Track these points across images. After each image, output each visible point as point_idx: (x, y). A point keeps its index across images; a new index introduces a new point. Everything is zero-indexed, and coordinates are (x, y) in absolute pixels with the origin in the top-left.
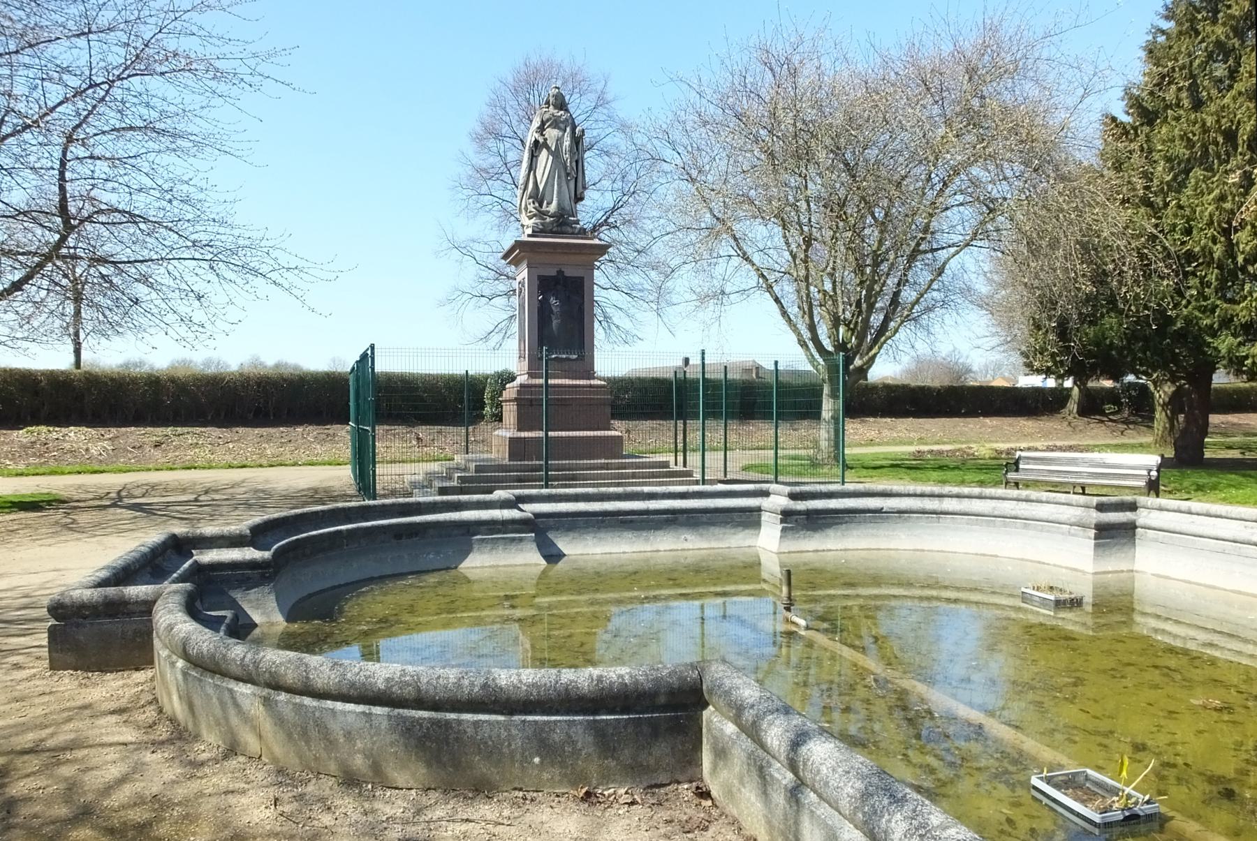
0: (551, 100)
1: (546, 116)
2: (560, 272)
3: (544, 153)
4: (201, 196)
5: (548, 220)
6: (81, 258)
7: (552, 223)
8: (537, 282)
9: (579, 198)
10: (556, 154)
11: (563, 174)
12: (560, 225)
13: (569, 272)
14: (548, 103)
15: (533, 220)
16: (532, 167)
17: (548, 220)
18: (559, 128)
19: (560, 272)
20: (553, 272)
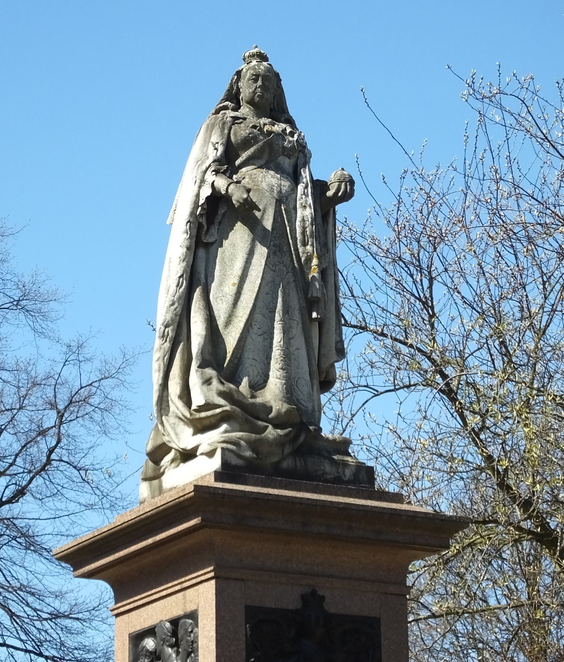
0: (246, 90)
1: (241, 132)
2: (312, 599)
3: (239, 237)
4: (83, 597)
5: (271, 433)
6: (479, 405)
7: (280, 442)
8: (242, 631)
9: (326, 383)
10: (277, 241)
11: (295, 303)
12: (298, 452)
13: (341, 601)
14: (233, 96)
15: (215, 436)
16: (197, 276)
17: (271, 433)
18: (279, 169)
19: (312, 599)
20: (287, 598)
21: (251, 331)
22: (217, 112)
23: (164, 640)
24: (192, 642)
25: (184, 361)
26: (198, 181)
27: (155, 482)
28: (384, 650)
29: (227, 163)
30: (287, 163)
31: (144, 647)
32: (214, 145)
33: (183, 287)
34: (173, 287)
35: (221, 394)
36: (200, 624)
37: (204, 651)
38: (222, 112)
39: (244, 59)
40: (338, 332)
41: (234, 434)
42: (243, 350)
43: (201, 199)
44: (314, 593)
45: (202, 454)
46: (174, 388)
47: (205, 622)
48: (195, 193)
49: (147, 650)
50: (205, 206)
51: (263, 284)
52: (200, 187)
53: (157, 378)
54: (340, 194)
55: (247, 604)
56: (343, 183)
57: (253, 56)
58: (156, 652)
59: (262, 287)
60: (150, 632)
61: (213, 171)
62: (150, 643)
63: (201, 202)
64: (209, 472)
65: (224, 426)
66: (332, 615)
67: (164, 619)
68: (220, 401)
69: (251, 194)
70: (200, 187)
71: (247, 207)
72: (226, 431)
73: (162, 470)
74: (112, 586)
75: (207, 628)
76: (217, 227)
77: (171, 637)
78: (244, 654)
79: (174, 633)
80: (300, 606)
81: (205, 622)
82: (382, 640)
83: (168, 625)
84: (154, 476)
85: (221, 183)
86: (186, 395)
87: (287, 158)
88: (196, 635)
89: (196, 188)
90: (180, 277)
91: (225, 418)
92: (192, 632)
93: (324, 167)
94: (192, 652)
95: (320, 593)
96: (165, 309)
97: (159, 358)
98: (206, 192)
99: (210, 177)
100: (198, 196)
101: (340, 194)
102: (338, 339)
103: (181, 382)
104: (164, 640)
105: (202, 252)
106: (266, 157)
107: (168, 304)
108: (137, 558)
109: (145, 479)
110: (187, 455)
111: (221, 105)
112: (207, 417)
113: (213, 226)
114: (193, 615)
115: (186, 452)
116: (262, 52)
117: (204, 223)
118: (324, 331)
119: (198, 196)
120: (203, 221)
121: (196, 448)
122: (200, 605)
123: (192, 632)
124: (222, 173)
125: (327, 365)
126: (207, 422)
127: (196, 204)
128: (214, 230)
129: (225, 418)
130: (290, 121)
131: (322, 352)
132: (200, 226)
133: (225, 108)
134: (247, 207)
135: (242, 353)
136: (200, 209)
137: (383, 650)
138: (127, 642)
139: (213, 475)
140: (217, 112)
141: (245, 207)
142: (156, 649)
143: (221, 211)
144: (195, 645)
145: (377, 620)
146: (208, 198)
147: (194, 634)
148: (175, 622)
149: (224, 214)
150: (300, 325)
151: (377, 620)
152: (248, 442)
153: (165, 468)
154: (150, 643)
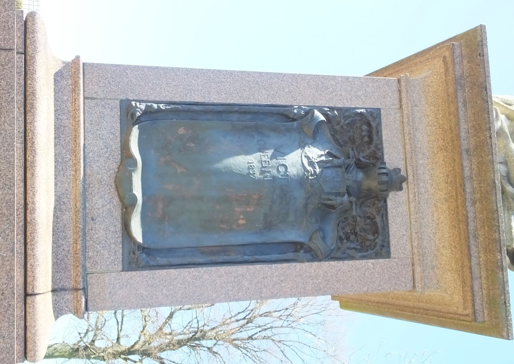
78: (340, 106)
95: (404, 185)
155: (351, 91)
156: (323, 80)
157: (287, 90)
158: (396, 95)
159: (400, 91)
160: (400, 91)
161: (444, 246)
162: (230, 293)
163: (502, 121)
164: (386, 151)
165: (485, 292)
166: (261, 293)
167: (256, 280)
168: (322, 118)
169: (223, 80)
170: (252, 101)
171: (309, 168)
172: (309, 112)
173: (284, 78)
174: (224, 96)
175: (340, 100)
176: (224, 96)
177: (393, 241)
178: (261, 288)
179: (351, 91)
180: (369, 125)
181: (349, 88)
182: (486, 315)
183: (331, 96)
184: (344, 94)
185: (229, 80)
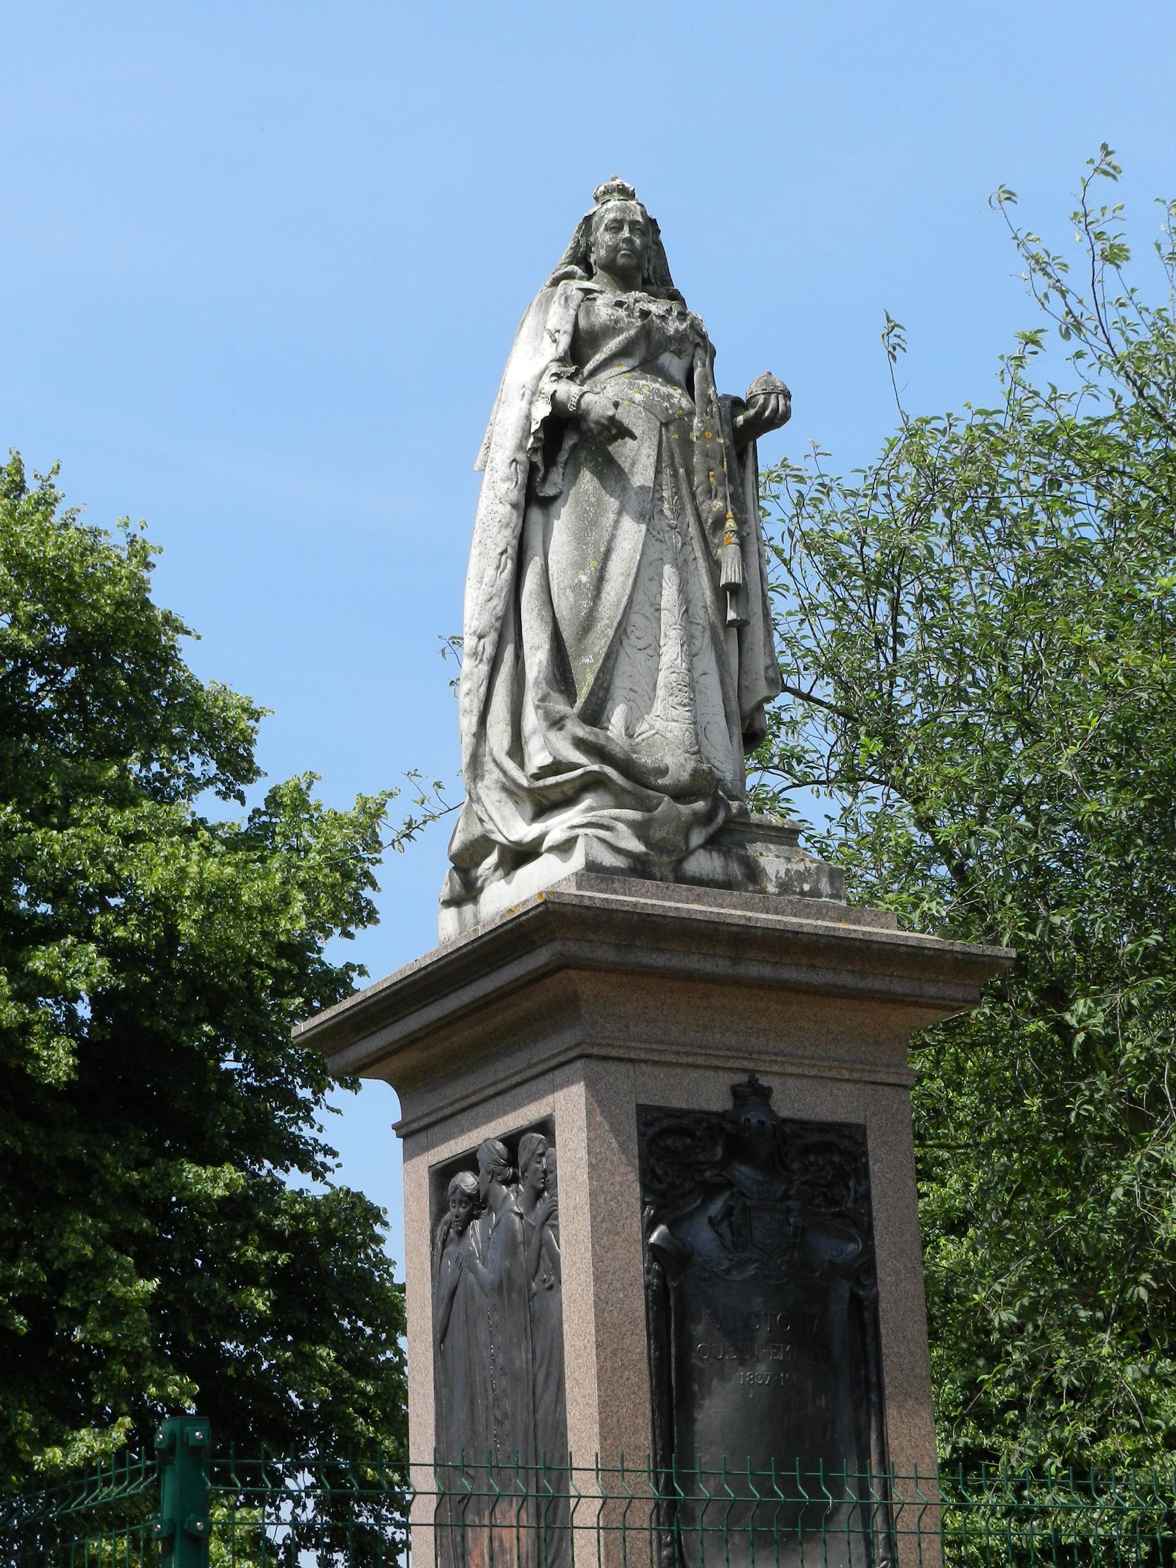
20: (710, 1094)
21: (625, 642)
22: (556, 282)
23: (493, 1174)
24: (545, 1172)
25: (546, 623)
26: (528, 393)
27: (468, 909)
28: (874, 1180)
29: (578, 351)
30: (672, 363)
31: (457, 1187)
32: (552, 335)
33: (506, 571)
34: (490, 572)
35: (580, 744)
36: (558, 1139)
37: (568, 1186)
38: (563, 283)
39: (597, 199)
40: (767, 650)
41: (606, 812)
42: (612, 674)
43: (533, 423)
44: (753, 1083)
45: (551, 849)
46: (499, 737)
47: (566, 1135)
48: (523, 413)
49: (463, 1193)
50: (541, 435)
51: (644, 563)
52: (531, 403)
53: (469, 724)
54: (767, 413)
55: (640, 1102)
56: (773, 396)
57: (608, 191)
58: (478, 1191)
59: (642, 569)
60: (468, 1161)
61: (553, 375)
62: (467, 1181)
63: (535, 427)
64: (565, 875)
65: (588, 801)
66: (785, 1121)
67: (492, 1136)
68: (577, 757)
69: (620, 410)
70: (531, 403)
71: (614, 431)
72: (591, 809)
73: (479, 883)
74: (397, 1088)
75: (572, 1146)
76: (561, 470)
77: (505, 1166)
78: (638, 1189)
79: (512, 1160)
80: (729, 1105)
81: (566, 1135)
82: (871, 1163)
83: (500, 1146)
84: (466, 892)
85: (568, 391)
86: (517, 750)
87: (676, 358)
88: (551, 1160)
89: (524, 404)
90: (502, 554)
91: (592, 783)
92: (542, 1155)
93: (734, 377)
94: (543, 1190)
95: (764, 1081)
96: (478, 609)
97: (470, 690)
98: (543, 410)
99: (548, 386)
100: (528, 417)
101: (767, 413)
102: (769, 662)
103: (509, 728)
104: (493, 1174)
105: (536, 515)
106: (641, 352)
107: (481, 599)
108: (442, 1033)
109: (447, 903)
110: (519, 856)
111: (562, 271)
112: (558, 784)
113: (554, 469)
114: (545, 1127)
115: (518, 848)
116: (627, 185)
117: (540, 464)
118: (746, 646)
119: (528, 417)
120: (538, 459)
121: (541, 839)
122: (558, 1106)
123: (542, 1155)
124: (568, 378)
125: (753, 704)
126: (555, 796)
127: (527, 432)
128: (556, 475)
129: (592, 783)
130: (675, 296)
131: (743, 683)
132: (532, 469)
133: (569, 276)
134: (614, 431)
135: (611, 679)
136: (531, 440)
137: (873, 1180)
138: (426, 1182)
139: (573, 879)
140: (556, 282)
141: (610, 431)
142: (478, 1191)
143: (569, 442)
144: (550, 1177)
145: (861, 1129)
146: (545, 421)
147: (548, 1158)
148: (511, 1141)
149: (574, 449)
150: (708, 634)
151: (861, 1129)
152: (631, 824)
153: (485, 880)
154: (467, 1181)
155: (612, 1162)
156: (599, 1219)
157: (621, 1295)
158: (612, 1067)
159: (605, 1058)
160: (605, 1058)
161: (851, 1020)
162: (923, 1432)
163: (616, 819)
164: (704, 1106)
165: (941, 977)
166: (921, 1377)
167: (905, 1385)
168: (662, 1228)
169: (615, 1419)
170: (644, 1366)
171: (751, 1270)
172: (655, 1252)
173: (603, 1297)
174: (640, 1421)
175: (629, 1187)
176: (640, 1421)
177: (841, 1116)
178: (916, 1377)
179: (612, 1162)
180: (667, 1131)
181: (608, 1165)
182: (971, 982)
183: (624, 1205)
184: (618, 1179)
185: (615, 1409)
